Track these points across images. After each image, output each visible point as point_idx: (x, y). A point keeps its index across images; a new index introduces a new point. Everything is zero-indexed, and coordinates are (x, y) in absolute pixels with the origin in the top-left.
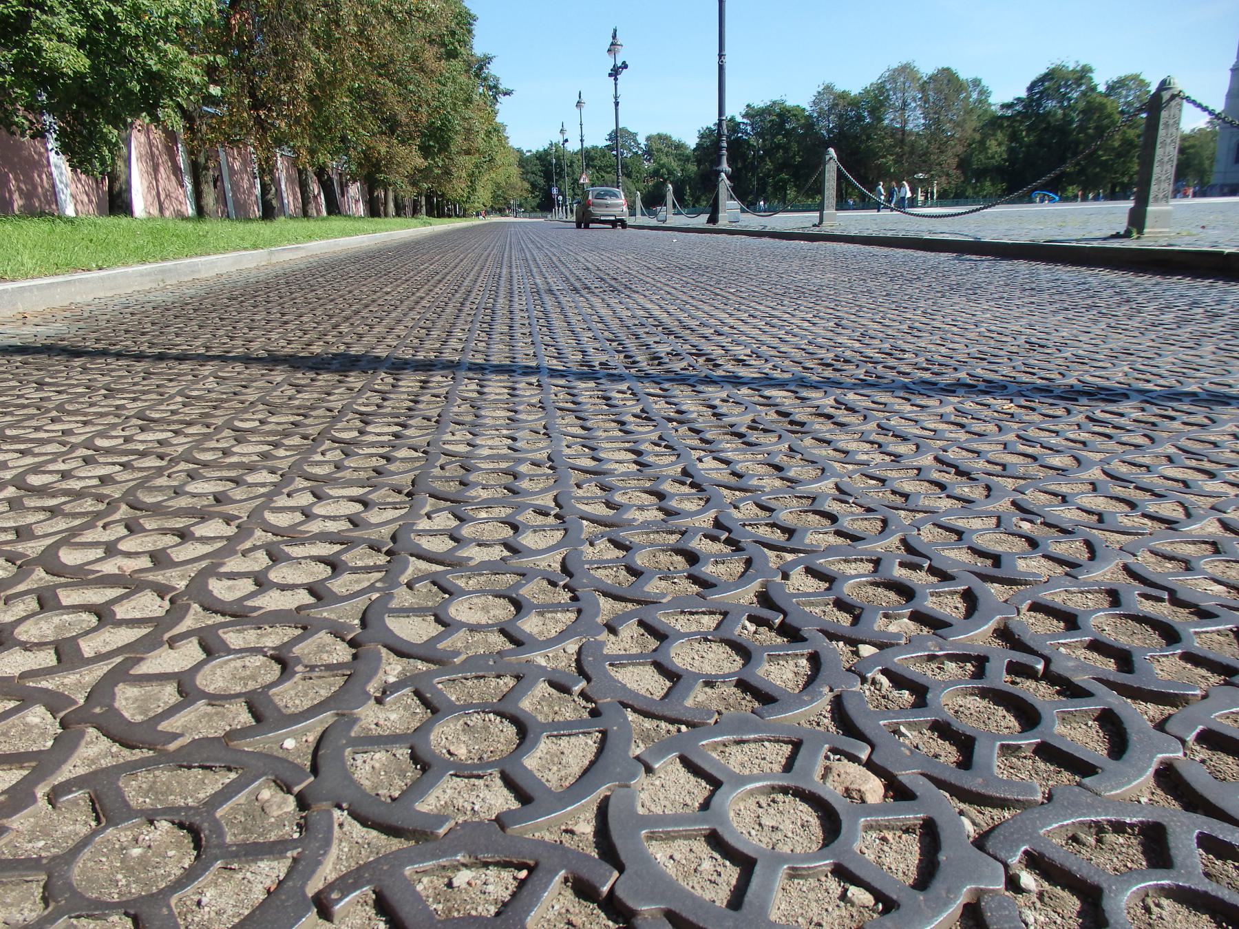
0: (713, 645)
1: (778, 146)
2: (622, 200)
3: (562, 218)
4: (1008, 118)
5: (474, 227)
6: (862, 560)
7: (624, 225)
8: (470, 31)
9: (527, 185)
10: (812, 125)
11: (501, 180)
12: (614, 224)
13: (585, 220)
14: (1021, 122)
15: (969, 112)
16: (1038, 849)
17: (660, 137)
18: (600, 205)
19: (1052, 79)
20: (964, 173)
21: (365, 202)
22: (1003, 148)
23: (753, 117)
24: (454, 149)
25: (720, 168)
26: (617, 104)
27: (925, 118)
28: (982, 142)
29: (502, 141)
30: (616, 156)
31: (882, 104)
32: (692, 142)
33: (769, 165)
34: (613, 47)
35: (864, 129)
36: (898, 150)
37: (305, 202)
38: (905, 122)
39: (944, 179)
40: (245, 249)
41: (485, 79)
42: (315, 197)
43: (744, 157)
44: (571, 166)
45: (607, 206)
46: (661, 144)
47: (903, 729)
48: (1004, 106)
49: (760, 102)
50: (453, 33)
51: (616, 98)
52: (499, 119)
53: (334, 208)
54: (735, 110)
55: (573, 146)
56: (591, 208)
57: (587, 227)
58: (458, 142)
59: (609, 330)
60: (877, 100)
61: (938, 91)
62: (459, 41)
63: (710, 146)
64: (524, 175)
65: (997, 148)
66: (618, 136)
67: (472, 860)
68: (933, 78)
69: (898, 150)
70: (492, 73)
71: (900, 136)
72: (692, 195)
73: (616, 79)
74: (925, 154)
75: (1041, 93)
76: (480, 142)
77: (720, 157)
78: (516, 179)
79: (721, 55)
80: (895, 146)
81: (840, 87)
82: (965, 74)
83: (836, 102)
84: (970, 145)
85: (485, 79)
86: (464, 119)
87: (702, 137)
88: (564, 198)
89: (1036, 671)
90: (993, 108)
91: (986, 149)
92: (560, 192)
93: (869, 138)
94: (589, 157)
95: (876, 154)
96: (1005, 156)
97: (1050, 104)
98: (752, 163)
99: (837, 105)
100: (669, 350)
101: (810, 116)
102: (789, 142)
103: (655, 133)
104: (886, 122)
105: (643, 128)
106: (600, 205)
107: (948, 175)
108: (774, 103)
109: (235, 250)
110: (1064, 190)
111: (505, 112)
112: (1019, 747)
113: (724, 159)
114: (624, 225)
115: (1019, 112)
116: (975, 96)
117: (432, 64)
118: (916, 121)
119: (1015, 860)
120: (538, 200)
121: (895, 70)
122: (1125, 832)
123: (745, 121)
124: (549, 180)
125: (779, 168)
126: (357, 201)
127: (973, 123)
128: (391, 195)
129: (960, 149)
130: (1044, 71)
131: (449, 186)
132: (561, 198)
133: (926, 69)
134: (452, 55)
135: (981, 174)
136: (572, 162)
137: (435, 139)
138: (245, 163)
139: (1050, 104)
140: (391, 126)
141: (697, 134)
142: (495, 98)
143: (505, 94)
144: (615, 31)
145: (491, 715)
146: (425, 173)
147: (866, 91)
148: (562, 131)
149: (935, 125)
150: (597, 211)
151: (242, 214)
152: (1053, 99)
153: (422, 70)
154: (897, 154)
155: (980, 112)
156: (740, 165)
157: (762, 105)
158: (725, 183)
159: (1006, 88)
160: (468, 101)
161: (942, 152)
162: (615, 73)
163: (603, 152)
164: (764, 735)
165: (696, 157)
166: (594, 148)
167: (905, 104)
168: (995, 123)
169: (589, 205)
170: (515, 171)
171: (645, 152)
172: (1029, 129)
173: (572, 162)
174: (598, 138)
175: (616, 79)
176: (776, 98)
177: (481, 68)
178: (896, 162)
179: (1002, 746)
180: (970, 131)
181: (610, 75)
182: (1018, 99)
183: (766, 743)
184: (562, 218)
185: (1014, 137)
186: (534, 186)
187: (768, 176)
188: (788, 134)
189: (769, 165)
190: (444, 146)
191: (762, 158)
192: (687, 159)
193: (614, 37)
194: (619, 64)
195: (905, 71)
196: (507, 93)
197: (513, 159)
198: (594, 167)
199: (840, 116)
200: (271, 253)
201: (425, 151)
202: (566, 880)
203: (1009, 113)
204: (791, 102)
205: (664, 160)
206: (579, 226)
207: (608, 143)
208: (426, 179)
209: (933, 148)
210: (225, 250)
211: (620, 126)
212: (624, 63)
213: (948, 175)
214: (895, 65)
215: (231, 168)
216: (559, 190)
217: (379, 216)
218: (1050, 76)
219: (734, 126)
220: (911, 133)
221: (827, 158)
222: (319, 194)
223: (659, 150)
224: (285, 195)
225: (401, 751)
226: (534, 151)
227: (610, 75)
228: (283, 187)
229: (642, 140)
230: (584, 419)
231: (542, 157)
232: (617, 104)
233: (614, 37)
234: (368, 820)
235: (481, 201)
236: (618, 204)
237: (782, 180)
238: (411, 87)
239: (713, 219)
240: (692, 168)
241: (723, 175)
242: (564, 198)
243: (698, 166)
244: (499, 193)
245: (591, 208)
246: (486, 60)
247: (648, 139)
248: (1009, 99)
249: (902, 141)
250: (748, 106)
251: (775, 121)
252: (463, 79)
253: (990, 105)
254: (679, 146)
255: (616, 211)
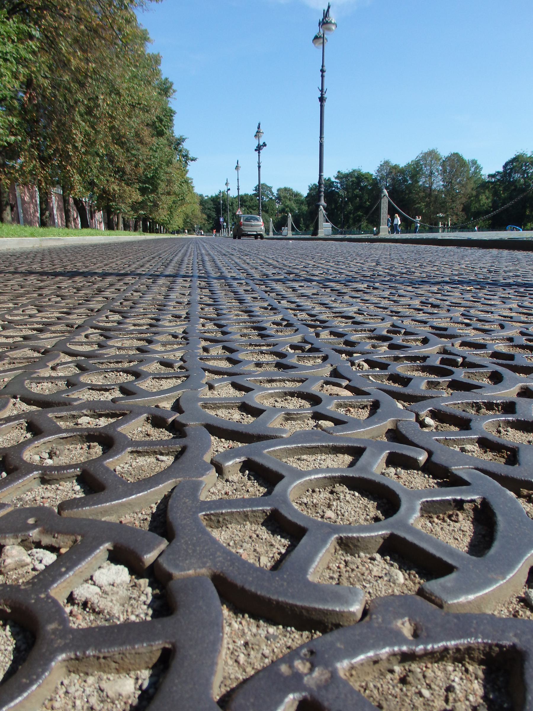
0: (266, 355)
1: (356, 196)
2: (261, 222)
3: (227, 233)
4: (492, 183)
5: (171, 238)
6: (365, 331)
7: (262, 237)
8: (171, 120)
9: (205, 216)
10: (377, 183)
11: (189, 212)
12: (256, 236)
13: (239, 234)
14: (500, 186)
15: (469, 179)
16: (438, 408)
17: (286, 189)
18: (247, 225)
19: (518, 161)
20: (467, 214)
21: (105, 223)
22: (490, 200)
23: (342, 178)
24: (160, 190)
25: (320, 203)
26: (259, 167)
27: (443, 181)
28: (477, 196)
29: (190, 189)
30: (259, 200)
31: (418, 173)
32: (304, 192)
33: (350, 207)
34: (258, 134)
35: (408, 187)
36: (427, 199)
37: (68, 220)
38: (432, 183)
39: (454, 217)
40: (26, 236)
41: (181, 151)
42: (74, 219)
43: (336, 202)
44: (232, 205)
45: (252, 226)
46: (286, 194)
47: (370, 377)
48: (489, 176)
49: (346, 170)
50: (161, 121)
51: (259, 163)
52: (188, 175)
53: (85, 225)
54: (330, 174)
55: (233, 193)
56: (242, 227)
57: (239, 238)
58: (162, 187)
59: (239, 265)
60: (415, 170)
61: (452, 167)
62: (164, 126)
63: (315, 193)
64: (203, 211)
65: (485, 200)
66: (260, 189)
67: (92, 413)
68: (448, 159)
69: (427, 199)
70: (185, 147)
71: (429, 192)
72: (304, 224)
73: (259, 153)
74: (444, 202)
75: (511, 169)
76: (176, 188)
77: (320, 197)
78: (198, 212)
79: (321, 138)
80: (426, 197)
81: (393, 162)
82: (467, 157)
83: (391, 172)
84: (470, 198)
85: (181, 151)
86: (166, 173)
87: (311, 189)
88: (227, 224)
89: (457, 362)
90: (483, 177)
91: (479, 201)
92: (225, 221)
93: (410, 192)
94: (243, 200)
95: (415, 201)
96: (490, 205)
97: (517, 176)
98: (341, 206)
99: (392, 172)
100: (297, 339)
101: (376, 179)
102: (363, 194)
103: (283, 187)
104: (421, 183)
105: (276, 183)
106: (247, 225)
107: (457, 215)
108: (354, 171)
109: (19, 236)
110: (525, 225)
111: (193, 171)
112: (439, 383)
113: (322, 198)
114: (262, 237)
115: (499, 180)
116: (473, 169)
117: (148, 140)
118: (438, 183)
119: (423, 413)
120: (211, 225)
121: (426, 154)
122: (493, 409)
123: (337, 181)
124: (219, 213)
125: (357, 209)
126: (100, 223)
127: (471, 185)
128: (121, 220)
129: (464, 200)
130: (513, 156)
131: (156, 213)
132: (225, 224)
133: (444, 153)
134: (160, 134)
135: (477, 214)
136: (232, 203)
137: (149, 184)
138: (32, 197)
139: (517, 176)
140: (120, 172)
141: (308, 188)
142: (186, 162)
143: (192, 160)
144: (259, 124)
145: (121, 373)
146: (142, 205)
147: (409, 165)
148: (227, 184)
149: (449, 183)
150: (245, 229)
151: (29, 223)
152: (518, 173)
153: (141, 142)
154: (427, 202)
155: (475, 179)
156: (333, 206)
157: (347, 172)
158: (322, 212)
159: (491, 166)
160: (169, 163)
161: (453, 201)
162: (259, 149)
163: (251, 198)
164: (285, 378)
165: (307, 201)
166: (246, 195)
167: (431, 173)
168: (484, 185)
169: (241, 225)
170: (197, 207)
171: (277, 198)
172: (505, 190)
173: (232, 203)
174: (248, 189)
175: (259, 153)
176: (356, 168)
177: (179, 144)
178: (426, 206)
179: (428, 382)
180: (470, 190)
181: (256, 150)
182: (498, 172)
183: (287, 382)
184: (227, 233)
185: (496, 193)
186: (209, 217)
187: (350, 213)
188: (362, 189)
189: (350, 207)
190: (155, 190)
191: (346, 203)
192: (302, 203)
193: (259, 128)
194: (261, 144)
195: (432, 155)
196: (193, 160)
197: (197, 201)
198: (246, 206)
199: (393, 179)
200: (41, 240)
201: (143, 191)
202: (148, 418)
203: (493, 180)
204: (364, 171)
205: (288, 203)
206: (235, 238)
207: (255, 192)
208: (143, 209)
209: (448, 199)
210: (13, 236)
211: (262, 182)
212: (264, 143)
213: (457, 215)
214: (426, 150)
215: (23, 200)
216: (224, 219)
217: (112, 229)
218: (516, 159)
219: (329, 184)
220: (435, 190)
221: (383, 195)
222: (77, 217)
223: (285, 197)
224: (56, 217)
225: (61, 383)
226: (210, 196)
227: (256, 150)
228: (55, 212)
229: (275, 191)
230: (248, 390)
231: (215, 200)
232: (259, 167)
233: (259, 128)
234: (31, 400)
235: (177, 224)
236: (259, 225)
237: (359, 216)
238: (134, 152)
239: (315, 233)
240: (305, 208)
241: (321, 207)
242: (227, 224)
243: (308, 207)
244: (188, 220)
245: (242, 227)
246: (179, 141)
247: (278, 190)
248: (493, 172)
249: (430, 195)
250: (339, 172)
251: (355, 181)
252: (167, 149)
253: (481, 175)
254: (297, 195)
255: (257, 229)
